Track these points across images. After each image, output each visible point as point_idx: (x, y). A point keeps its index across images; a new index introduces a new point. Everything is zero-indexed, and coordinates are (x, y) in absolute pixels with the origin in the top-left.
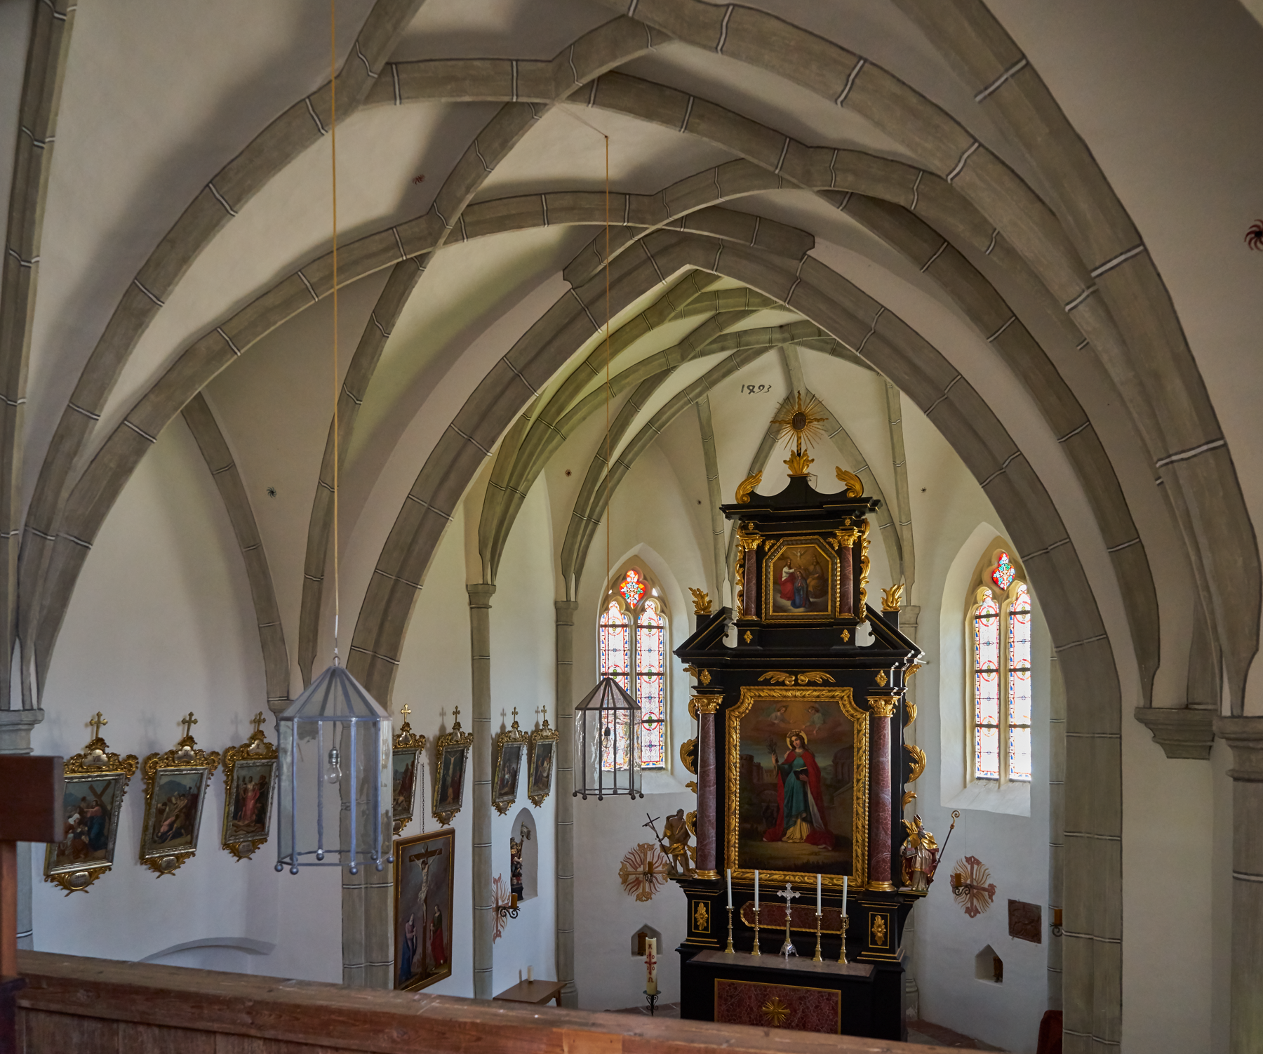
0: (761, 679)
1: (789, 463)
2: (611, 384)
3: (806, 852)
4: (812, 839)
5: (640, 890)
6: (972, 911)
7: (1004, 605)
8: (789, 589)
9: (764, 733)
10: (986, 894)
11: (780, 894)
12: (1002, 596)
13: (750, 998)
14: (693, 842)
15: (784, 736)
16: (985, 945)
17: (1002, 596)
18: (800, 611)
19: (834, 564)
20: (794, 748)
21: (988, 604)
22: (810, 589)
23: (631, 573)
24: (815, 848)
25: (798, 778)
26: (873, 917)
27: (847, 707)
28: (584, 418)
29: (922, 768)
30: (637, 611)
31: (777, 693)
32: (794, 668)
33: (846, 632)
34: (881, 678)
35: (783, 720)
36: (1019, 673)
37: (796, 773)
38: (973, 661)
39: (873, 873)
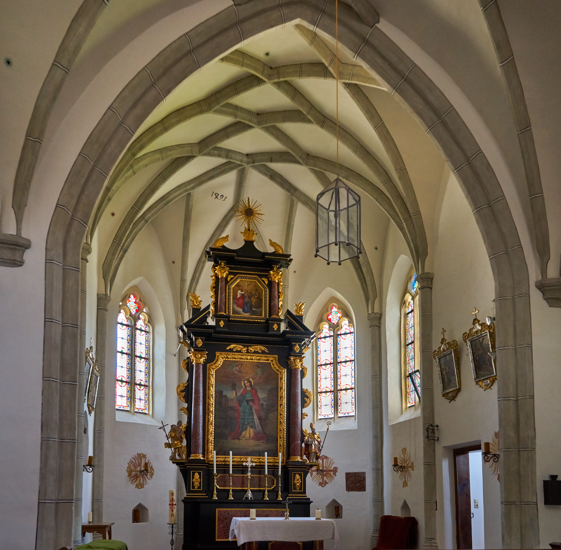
0: (228, 348)
1: (244, 233)
2: (161, 151)
3: (252, 444)
4: (257, 437)
5: (138, 482)
6: (323, 484)
8: (242, 302)
9: (227, 378)
10: (332, 472)
11: (244, 464)
16: (331, 500)
17: (335, 327)
18: (247, 315)
19: (265, 291)
20: (246, 387)
21: (326, 330)
22: (253, 303)
23: (132, 296)
24: (257, 443)
25: (248, 404)
26: (295, 474)
27: (275, 366)
28: (146, 166)
30: (136, 318)
31: (237, 356)
32: (247, 342)
34: (297, 348)
35: (240, 372)
36: (343, 364)
37: (248, 401)
39: (289, 453)
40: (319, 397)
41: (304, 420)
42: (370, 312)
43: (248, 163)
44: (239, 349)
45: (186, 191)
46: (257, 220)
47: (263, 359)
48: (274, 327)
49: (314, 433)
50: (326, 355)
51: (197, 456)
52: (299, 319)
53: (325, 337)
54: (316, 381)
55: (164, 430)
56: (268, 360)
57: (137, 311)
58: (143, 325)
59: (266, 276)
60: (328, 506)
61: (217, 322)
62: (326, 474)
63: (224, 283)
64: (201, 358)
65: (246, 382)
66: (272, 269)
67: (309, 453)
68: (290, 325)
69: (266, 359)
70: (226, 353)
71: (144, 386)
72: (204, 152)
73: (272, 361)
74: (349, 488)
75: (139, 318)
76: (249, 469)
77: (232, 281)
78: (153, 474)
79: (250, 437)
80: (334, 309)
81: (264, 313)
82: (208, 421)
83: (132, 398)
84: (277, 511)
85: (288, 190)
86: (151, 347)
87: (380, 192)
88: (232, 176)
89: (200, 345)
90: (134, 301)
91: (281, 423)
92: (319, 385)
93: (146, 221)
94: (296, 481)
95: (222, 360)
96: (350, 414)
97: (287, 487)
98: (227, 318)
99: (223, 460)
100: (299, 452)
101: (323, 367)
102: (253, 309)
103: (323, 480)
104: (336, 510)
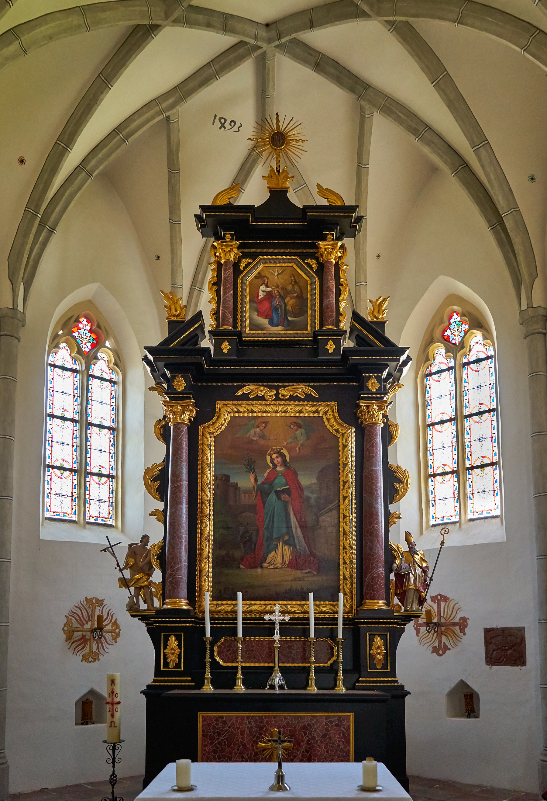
0: (239, 393)
3: (290, 578)
5: (87, 650)
6: (440, 650)
7: (459, 355)
8: (270, 308)
9: (241, 451)
10: (457, 628)
11: (267, 617)
12: (454, 349)
13: (242, 732)
14: (157, 576)
15: (264, 454)
18: (278, 330)
20: (275, 466)
21: (440, 358)
22: (289, 308)
24: (299, 574)
25: (279, 498)
26: (372, 637)
27: (332, 423)
29: (406, 490)
30: (90, 358)
31: (257, 407)
33: (331, 343)
34: (373, 385)
35: (263, 437)
37: (278, 493)
38: (425, 416)
39: (363, 592)
40: (430, 484)
41: (392, 529)
42: (524, 307)
43: (270, 41)
44: (260, 394)
45: (161, 112)
46: (293, 151)
47: (308, 410)
48: (328, 347)
49: (412, 551)
50: (441, 406)
51: (175, 603)
52: (377, 328)
53: (440, 372)
54: (423, 453)
55: (113, 554)
56: (317, 412)
57: (93, 346)
58: (107, 370)
59: (313, 256)
60: (451, 694)
61: (217, 345)
62: (444, 630)
63: (231, 271)
64: (183, 413)
65: (274, 456)
66: (323, 238)
67: (405, 592)
68: (360, 340)
69: (314, 409)
70: (236, 402)
71: (108, 476)
72: (176, 15)
73: (326, 413)
74: (492, 659)
75: (96, 358)
76: (277, 629)
77: (248, 269)
78: (118, 635)
79: (284, 563)
80: (456, 318)
81: (311, 322)
82: (201, 534)
83: (82, 497)
84: (327, 718)
85: (352, 90)
86: (120, 409)
87: (533, 30)
88: (243, 76)
89: (180, 389)
90: (88, 328)
91: (345, 533)
92: (430, 462)
93: (90, 174)
94: (374, 651)
95: (228, 417)
96: (492, 514)
97: (357, 663)
98: (236, 336)
99: (230, 609)
100: (382, 591)
101: (437, 427)
102: (290, 319)
103: (440, 642)
104: (467, 701)
